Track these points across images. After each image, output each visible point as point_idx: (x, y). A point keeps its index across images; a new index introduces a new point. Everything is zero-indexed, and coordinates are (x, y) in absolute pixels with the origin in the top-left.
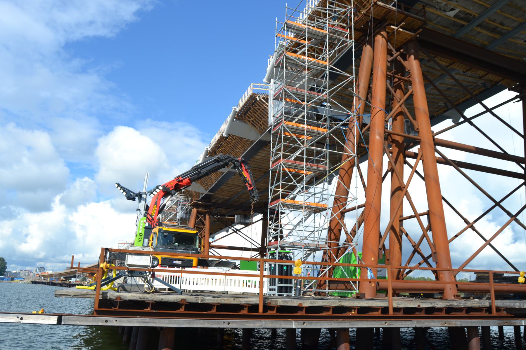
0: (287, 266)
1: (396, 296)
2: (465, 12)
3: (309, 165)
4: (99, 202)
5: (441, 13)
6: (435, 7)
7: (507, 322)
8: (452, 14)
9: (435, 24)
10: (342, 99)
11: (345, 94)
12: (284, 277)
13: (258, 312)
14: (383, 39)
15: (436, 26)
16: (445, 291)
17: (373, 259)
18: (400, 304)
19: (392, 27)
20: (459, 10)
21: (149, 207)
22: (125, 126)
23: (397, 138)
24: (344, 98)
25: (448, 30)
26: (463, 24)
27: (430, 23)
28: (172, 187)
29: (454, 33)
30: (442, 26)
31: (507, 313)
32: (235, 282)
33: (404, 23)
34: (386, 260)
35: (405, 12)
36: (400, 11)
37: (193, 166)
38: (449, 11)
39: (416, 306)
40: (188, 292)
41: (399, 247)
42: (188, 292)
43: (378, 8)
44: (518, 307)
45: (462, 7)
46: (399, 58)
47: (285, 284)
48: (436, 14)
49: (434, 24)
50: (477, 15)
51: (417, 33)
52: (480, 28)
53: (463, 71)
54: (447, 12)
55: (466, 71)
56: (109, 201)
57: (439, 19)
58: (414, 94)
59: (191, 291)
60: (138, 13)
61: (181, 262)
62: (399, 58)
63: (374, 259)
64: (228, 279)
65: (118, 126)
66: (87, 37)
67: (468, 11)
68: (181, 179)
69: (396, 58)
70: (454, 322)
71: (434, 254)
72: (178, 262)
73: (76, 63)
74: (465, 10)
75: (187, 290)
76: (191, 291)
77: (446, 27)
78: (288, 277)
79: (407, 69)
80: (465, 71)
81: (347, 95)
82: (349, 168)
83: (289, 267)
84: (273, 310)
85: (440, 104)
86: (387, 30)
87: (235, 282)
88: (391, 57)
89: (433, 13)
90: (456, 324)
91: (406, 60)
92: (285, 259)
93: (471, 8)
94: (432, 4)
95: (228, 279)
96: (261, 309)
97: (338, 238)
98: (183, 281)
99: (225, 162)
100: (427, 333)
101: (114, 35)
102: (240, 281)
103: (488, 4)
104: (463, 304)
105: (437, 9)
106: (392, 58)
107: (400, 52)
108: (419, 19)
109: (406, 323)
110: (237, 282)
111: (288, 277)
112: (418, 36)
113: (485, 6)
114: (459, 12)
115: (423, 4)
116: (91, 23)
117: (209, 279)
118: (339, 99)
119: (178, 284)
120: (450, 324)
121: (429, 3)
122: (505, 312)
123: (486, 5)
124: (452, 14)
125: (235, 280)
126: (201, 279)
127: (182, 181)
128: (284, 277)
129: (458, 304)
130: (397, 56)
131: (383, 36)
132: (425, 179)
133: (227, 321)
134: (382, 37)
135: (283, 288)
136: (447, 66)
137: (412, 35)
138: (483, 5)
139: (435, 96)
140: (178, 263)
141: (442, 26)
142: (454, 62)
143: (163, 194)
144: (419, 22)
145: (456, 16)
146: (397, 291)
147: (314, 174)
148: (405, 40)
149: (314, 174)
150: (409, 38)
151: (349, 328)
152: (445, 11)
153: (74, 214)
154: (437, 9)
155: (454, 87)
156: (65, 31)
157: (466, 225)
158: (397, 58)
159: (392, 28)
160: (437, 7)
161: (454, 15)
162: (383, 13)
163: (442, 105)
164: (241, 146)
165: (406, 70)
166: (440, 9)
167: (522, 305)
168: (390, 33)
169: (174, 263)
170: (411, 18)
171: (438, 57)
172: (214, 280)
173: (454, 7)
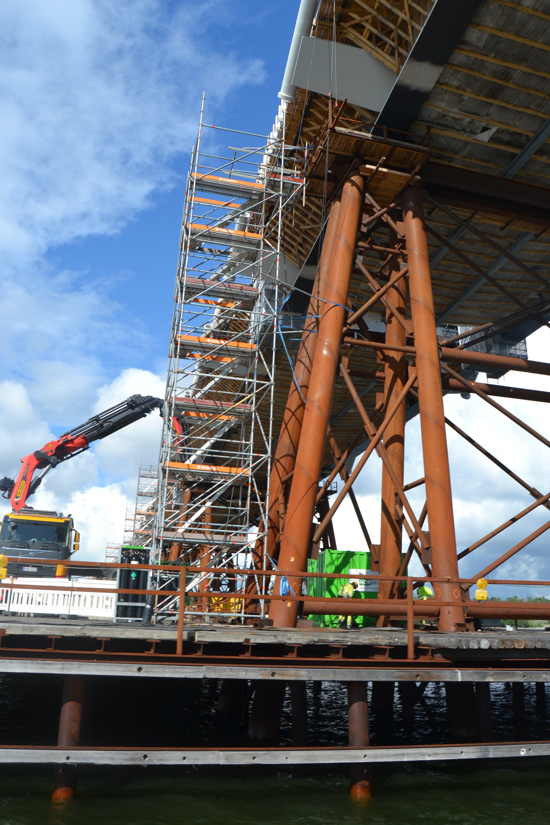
0: (138, 573)
1: (389, 625)
2: (509, 131)
3: (219, 405)
4: (105, 486)
5: (468, 136)
6: (453, 128)
7: (420, 674)
8: (485, 137)
9: (466, 158)
10: (358, 298)
11: (362, 290)
12: (131, 591)
13: (175, 653)
14: (354, 187)
15: (468, 160)
16: (440, 617)
17: (292, 560)
18: (204, 637)
19: (368, 166)
20: (497, 128)
21: (15, 484)
22: (138, 368)
23: (392, 354)
24: (361, 296)
25: (490, 165)
26: (513, 153)
27: (456, 157)
28: (52, 451)
29: (502, 169)
30: (478, 160)
31: (444, 658)
32: (85, 600)
33: (385, 158)
34: (373, 563)
35: (390, 140)
36: (379, 139)
37: (91, 418)
38: (481, 132)
39: (241, 640)
40: (26, 616)
41: (395, 539)
42: (26, 616)
43: (340, 138)
44: (454, 646)
45: (501, 123)
46: (387, 218)
47: (133, 601)
48: (460, 140)
49: (463, 157)
50: (531, 135)
51: (413, 172)
52: (546, 157)
53: (536, 234)
54: (477, 134)
55: (540, 234)
56: (118, 484)
57: (469, 147)
58: (410, 276)
59: (32, 615)
60: (153, 196)
61: (36, 568)
62: (387, 218)
63: (295, 559)
64: (75, 595)
65: (128, 368)
66: (79, 237)
67: (513, 129)
68: (70, 437)
69: (379, 217)
70: (293, 672)
71: (426, 551)
72: (31, 568)
73: (65, 277)
74: (507, 127)
75: (24, 613)
76: (32, 615)
77: (487, 161)
78: (139, 592)
79: (400, 235)
80: (538, 233)
81: (365, 291)
82: (299, 407)
83: (142, 574)
84: (338, 653)
85: (530, 297)
86: (361, 173)
87: (85, 600)
88: (370, 217)
89: (454, 139)
90: (297, 676)
91: (402, 220)
92: (135, 560)
93: (518, 123)
94: (446, 123)
95: (75, 595)
96: (179, 648)
97: (276, 525)
98: (32, 598)
99: (143, 407)
100: (527, 697)
101: (118, 232)
102: (94, 598)
103: (543, 113)
104: (352, 638)
105: (459, 130)
106: (372, 218)
107: (389, 208)
108: (418, 150)
109: (184, 671)
110: (89, 599)
111: (139, 592)
112: (419, 177)
113: (540, 117)
114: (497, 131)
115: (427, 124)
116: (84, 216)
117: (15, 594)
118: (355, 299)
119: (6, 602)
120: (283, 675)
121: (441, 122)
122: (439, 655)
123: (541, 115)
124: (485, 137)
125: (98, 597)
126: (105, 598)
127: (72, 441)
128: (131, 591)
129: (337, 639)
130: (382, 215)
131: (354, 184)
132: (443, 420)
133: (136, 666)
134: (352, 186)
135: (130, 609)
136: (502, 229)
137: (408, 177)
138: (536, 116)
139: (515, 283)
140: (30, 570)
141: (478, 160)
142: (511, 221)
143: (36, 462)
144: (421, 154)
145: (493, 139)
146: (392, 617)
147: (237, 419)
148: (400, 187)
149: (237, 419)
150: (404, 182)
151: (394, 682)
152: (473, 133)
153: (69, 505)
154: (459, 130)
155: (544, 265)
156: (47, 230)
157: (534, 501)
158: (382, 218)
159: (368, 168)
160: (457, 127)
161: (488, 138)
162: (352, 145)
163: (534, 297)
164: (232, 385)
165: (399, 237)
166: (464, 131)
167: (463, 643)
168: (368, 177)
169: (25, 570)
170: (404, 150)
171: (478, 213)
172: (66, 596)
173: (488, 124)
